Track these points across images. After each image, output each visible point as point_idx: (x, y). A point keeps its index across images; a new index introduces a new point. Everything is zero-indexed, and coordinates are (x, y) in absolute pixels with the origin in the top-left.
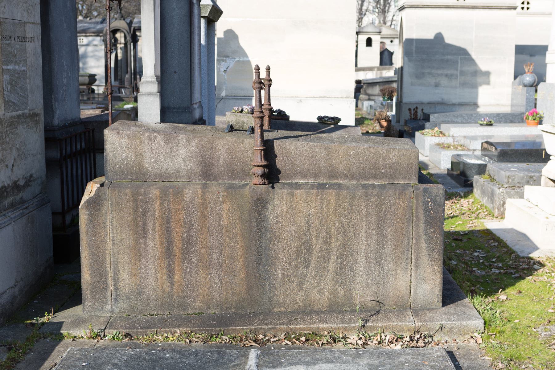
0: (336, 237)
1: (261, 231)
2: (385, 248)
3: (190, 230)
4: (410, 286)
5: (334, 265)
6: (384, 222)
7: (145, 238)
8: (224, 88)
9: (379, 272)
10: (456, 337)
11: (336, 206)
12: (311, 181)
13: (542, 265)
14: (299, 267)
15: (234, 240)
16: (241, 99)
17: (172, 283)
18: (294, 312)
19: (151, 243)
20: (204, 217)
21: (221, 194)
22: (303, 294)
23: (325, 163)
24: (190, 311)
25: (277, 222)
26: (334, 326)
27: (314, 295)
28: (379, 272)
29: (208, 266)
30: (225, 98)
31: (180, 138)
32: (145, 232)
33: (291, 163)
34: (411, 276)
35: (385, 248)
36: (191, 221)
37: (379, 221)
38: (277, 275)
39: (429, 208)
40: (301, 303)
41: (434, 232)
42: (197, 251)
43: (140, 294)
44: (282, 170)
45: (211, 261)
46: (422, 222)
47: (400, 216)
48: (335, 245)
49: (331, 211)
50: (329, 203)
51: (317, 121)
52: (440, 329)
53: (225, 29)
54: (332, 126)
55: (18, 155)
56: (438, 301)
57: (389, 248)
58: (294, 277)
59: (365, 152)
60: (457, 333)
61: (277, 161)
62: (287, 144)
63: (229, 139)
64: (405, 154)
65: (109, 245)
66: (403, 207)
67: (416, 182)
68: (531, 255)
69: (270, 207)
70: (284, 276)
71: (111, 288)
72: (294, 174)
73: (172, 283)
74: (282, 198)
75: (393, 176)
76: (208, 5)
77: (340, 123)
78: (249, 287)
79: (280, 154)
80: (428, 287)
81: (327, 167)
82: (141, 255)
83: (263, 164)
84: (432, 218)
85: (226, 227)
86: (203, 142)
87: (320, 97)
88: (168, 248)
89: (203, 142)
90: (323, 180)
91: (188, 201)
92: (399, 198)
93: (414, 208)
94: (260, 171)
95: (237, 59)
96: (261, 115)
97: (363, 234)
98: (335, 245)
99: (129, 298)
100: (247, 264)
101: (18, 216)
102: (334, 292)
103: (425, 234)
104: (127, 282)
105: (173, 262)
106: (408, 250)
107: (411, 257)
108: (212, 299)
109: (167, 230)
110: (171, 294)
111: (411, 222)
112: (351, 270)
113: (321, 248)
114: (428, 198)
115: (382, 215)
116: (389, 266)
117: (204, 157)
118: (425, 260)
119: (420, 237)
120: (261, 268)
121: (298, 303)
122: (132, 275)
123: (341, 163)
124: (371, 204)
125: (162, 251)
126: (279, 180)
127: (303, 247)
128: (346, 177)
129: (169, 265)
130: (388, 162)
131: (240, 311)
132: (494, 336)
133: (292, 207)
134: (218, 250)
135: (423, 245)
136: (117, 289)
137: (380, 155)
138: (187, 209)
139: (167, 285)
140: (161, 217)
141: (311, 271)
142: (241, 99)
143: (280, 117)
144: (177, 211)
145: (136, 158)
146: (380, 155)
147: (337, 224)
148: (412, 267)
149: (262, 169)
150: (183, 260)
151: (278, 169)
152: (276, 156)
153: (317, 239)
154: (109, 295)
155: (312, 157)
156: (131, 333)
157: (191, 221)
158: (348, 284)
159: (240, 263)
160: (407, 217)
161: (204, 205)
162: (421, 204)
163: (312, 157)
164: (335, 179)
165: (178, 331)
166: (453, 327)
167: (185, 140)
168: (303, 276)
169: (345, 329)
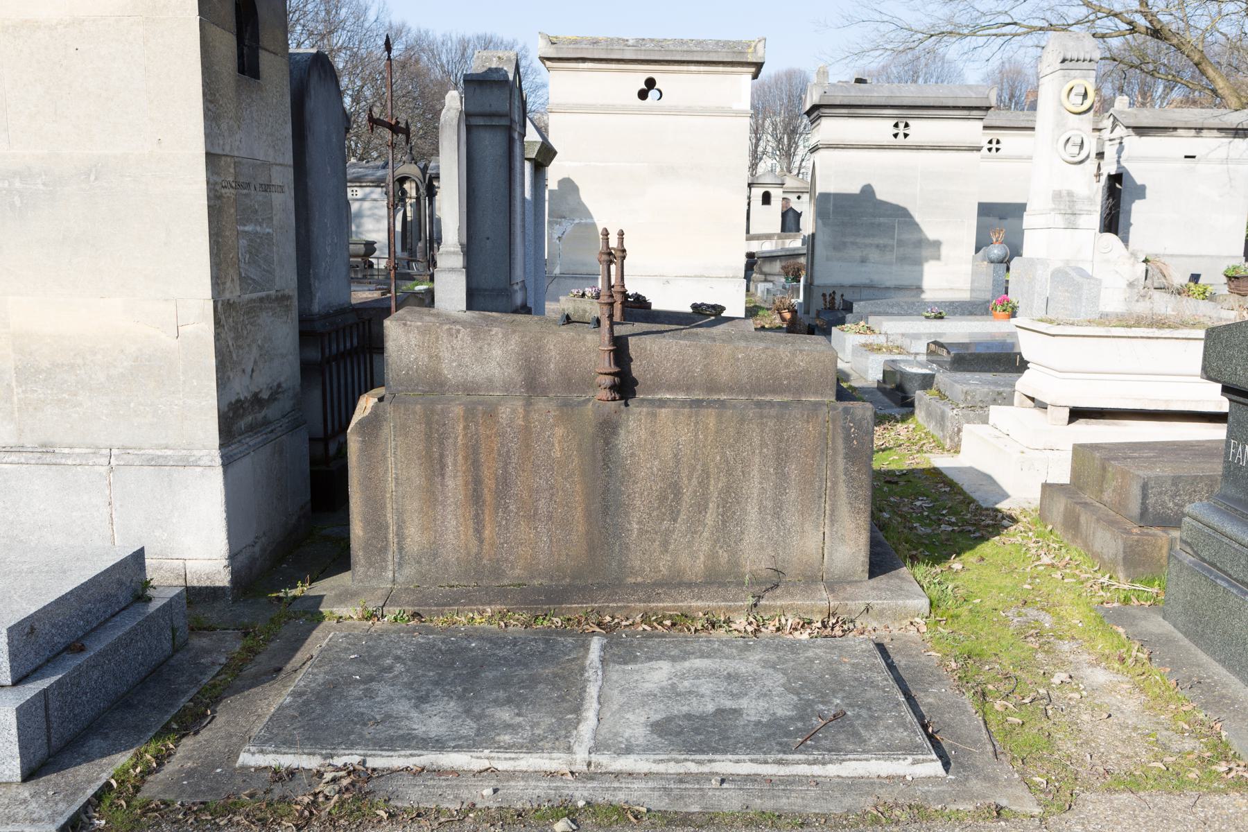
1: (608, 467)
4: (823, 549)
5: (714, 516)
7: (443, 475)
9: (779, 527)
10: (888, 622)
12: (681, 396)
13: (1014, 520)
14: (664, 520)
17: (481, 541)
19: (450, 483)
20: (528, 446)
22: (669, 559)
23: (702, 370)
24: (506, 582)
25: (633, 455)
27: (684, 561)
28: (779, 527)
29: (532, 517)
32: (443, 467)
34: (824, 533)
36: (508, 452)
37: (778, 454)
41: (858, 471)
43: (435, 555)
44: (640, 381)
45: (536, 509)
48: (715, 487)
49: (710, 439)
50: (707, 428)
53: (560, 178)
54: (713, 318)
56: (863, 571)
61: (632, 366)
63: (564, 334)
65: (391, 485)
67: (833, 399)
68: (998, 506)
69: (622, 432)
71: (393, 547)
72: (657, 387)
73: (481, 541)
75: (799, 391)
76: (535, 142)
79: (637, 357)
81: (705, 376)
82: (436, 500)
86: (527, 339)
87: (695, 276)
88: (475, 490)
89: (527, 339)
92: (808, 422)
93: (830, 436)
94: (608, 380)
95: (577, 221)
96: (610, 300)
97: (755, 473)
98: (715, 487)
102: (713, 556)
103: (845, 474)
106: (821, 497)
109: (474, 464)
110: (478, 557)
112: (737, 524)
113: (695, 492)
114: (850, 422)
115: (783, 445)
116: (792, 518)
117: (527, 360)
118: (844, 510)
120: (608, 520)
121: (660, 571)
122: (424, 529)
124: (767, 429)
126: (635, 395)
127: (669, 491)
128: (731, 390)
129: (477, 515)
130: (792, 369)
133: (653, 434)
134: (547, 494)
135: (842, 489)
136: (401, 549)
137: (782, 359)
140: (466, 446)
141: (680, 525)
144: (489, 437)
146: (782, 359)
147: (718, 458)
149: (612, 377)
152: (631, 360)
153: (690, 480)
154: (390, 558)
156: (421, 612)
157: (508, 452)
158: (733, 545)
159: (579, 514)
161: (527, 429)
164: (716, 394)
165: (489, 610)
166: (885, 609)
168: (669, 532)
169: (729, 609)
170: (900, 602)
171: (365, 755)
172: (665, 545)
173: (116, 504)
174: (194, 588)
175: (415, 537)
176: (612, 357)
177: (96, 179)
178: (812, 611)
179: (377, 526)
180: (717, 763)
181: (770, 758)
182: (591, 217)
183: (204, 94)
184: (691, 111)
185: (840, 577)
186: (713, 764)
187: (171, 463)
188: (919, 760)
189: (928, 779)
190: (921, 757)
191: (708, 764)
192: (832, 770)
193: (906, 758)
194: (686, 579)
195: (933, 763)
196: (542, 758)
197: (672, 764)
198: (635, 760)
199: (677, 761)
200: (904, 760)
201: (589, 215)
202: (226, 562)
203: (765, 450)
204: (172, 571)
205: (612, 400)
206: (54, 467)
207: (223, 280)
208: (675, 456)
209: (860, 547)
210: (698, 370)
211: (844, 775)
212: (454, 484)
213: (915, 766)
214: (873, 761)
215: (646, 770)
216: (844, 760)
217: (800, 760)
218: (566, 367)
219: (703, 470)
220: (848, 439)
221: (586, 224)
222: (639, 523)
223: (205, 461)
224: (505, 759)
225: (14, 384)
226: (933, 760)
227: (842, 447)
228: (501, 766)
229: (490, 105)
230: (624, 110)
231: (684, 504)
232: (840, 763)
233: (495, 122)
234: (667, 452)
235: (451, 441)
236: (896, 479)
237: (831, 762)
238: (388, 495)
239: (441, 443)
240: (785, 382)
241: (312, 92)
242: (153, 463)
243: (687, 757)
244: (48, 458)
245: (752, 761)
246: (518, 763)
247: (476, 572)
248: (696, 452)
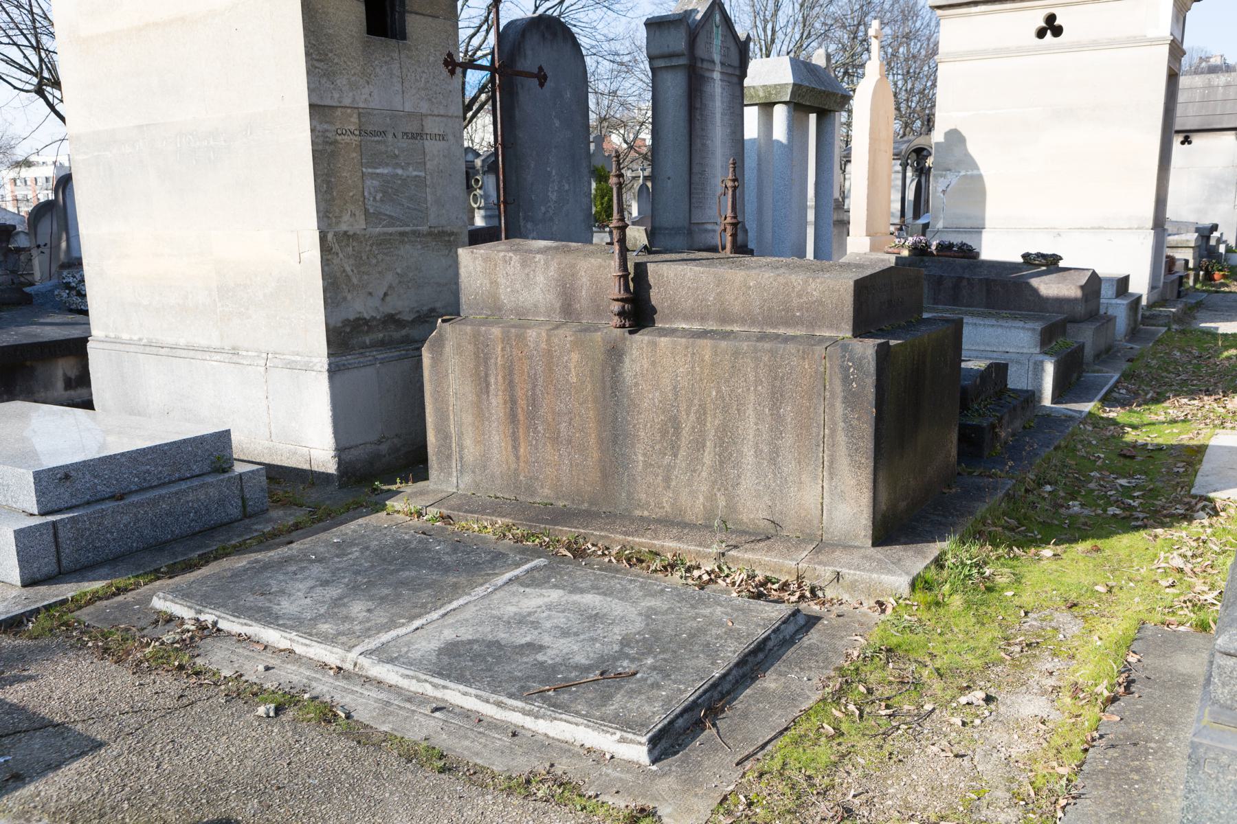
0: (712, 412)
1: (616, 395)
2: (783, 438)
3: (535, 386)
4: (822, 504)
5: (712, 455)
6: (781, 395)
7: (488, 392)
8: (942, 216)
9: (775, 475)
10: (863, 598)
11: (712, 365)
12: (696, 326)
13: (1215, 512)
14: (665, 454)
15: (584, 406)
16: (965, 232)
17: (518, 458)
18: (659, 521)
19: (494, 401)
20: (551, 370)
21: (569, 339)
22: (671, 495)
23: (715, 299)
24: (538, 500)
25: (636, 384)
26: (683, 546)
27: (684, 500)
28: (775, 475)
29: (555, 439)
30: (941, 231)
31: (537, 260)
32: (488, 385)
33: (670, 298)
34: (823, 487)
35: (783, 438)
36: (535, 374)
37: (773, 393)
38: (638, 462)
39: (849, 377)
40: (668, 508)
41: (858, 419)
42: (543, 416)
43: (485, 467)
44: (658, 308)
45: (559, 432)
46: (839, 400)
47: (805, 387)
48: (712, 425)
49: (706, 371)
50: (703, 360)
51: (1021, 260)
52: (836, 580)
53: (947, 130)
54: (1044, 268)
55: (400, 282)
56: (865, 536)
57: (789, 439)
58: (659, 467)
59: (771, 283)
60: (863, 592)
61: (651, 294)
62: (664, 269)
63: (593, 260)
64: (831, 286)
65: (452, 400)
66: (810, 372)
67: (849, 335)
68: (1212, 495)
69: (627, 360)
70: (647, 465)
71: (455, 456)
72: (676, 314)
73: (518, 458)
74: (642, 349)
75: (812, 324)
76: (787, 84)
77: (1062, 264)
78: (605, 476)
79: (655, 284)
80: (848, 509)
81: (718, 305)
82: (484, 415)
83: (620, 297)
84: (854, 394)
85: (575, 387)
86: (563, 265)
87: (1093, 228)
88: (512, 409)
89: (563, 265)
90: (711, 326)
91: (532, 346)
92: (804, 359)
93: (827, 377)
94: (616, 307)
95: (963, 173)
96: (620, 224)
97: (750, 412)
98: (712, 425)
99: (474, 472)
100: (601, 441)
101: (392, 357)
102: (711, 498)
103: (844, 421)
104: (472, 451)
105: (517, 428)
106: (819, 445)
107: (823, 457)
108: (561, 485)
109: (510, 385)
110: (516, 472)
111: (822, 399)
112: (734, 467)
113: (693, 428)
114: (848, 360)
115: (778, 383)
116: (789, 466)
117: (564, 286)
118: (843, 463)
119: (836, 424)
120: (617, 450)
121: (664, 507)
122: (477, 442)
123: (736, 299)
124: (762, 365)
125: (505, 412)
126: (654, 323)
127: (670, 425)
128: (743, 321)
129: (514, 433)
130: (805, 299)
131: (594, 509)
132: (916, 607)
133: (653, 364)
134: (566, 418)
135: (841, 438)
136: (461, 458)
137: (794, 287)
138: (531, 358)
139: (512, 458)
140: (504, 366)
141: (681, 462)
142: (965, 232)
143: (961, 254)
144: (520, 359)
145: (491, 287)
146: (794, 287)
147: (714, 393)
148: (825, 473)
149: (621, 304)
150: (528, 428)
151: (653, 306)
152: (650, 287)
153: (688, 415)
154: (454, 465)
155: (697, 289)
156: (452, 516)
157: (535, 374)
158: (730, 489)
159: (592, 440)
160: (815, 391)
161: (549, 352)
162: (837, 370)
163: (697, 289)
164: (729, 325)
165: (499, 522)
166: (857, 581)
167: (542, 262)
168: (669, 468)
169: (698, 553)
170: (875, 576)
171: (219, 617)
172: (667, 479)
173: (270, 398)
174: (315, 472)
175: (471, 451)
176: (622, 283)
177: (251, 133)
178: (781, 571)
179: (445, 437)
180: (449, 691)
181: (493, 697)
182: (978, 168)
183: (307, 54)
184: (1095, 45)
185: (840, 539)
186: (446, 691)
187: (299, 367)
188: (627, 738)
189: (629, 765)
190: (630, 736)
191: (442, 690)
192: (542, 726)
193: (615, 734)
194: (687, 520)
195: (639, 746)
196: (325, 650)
197: (414, 681)
198: (388, 670)
199: (419, 680)
200: (612, 734)
201: (974, 166)
202: (333, 453)
203: (760, 388)
204: (302, 456)
205: (620, 327)
206: (238, 366)
207: (337, 214)
208: (675, 388)
209: (862, 508)
210: (711, 299)
211: (551, 734)
212: (497, 402)
213: (620, 744)
214: (581, 728)
215: (393, 682)
216: (555, 719)
217: (517, 707)
218: (595, 293)
219: (700, 405)
220: (846, 380)
221: (972, 176)
222: (644, 455)
223: (318, 368)
224: (302, 644)
225: (217, 299)
226: (640, 743)
227: (840, 389)
228: (299, 650)
229: (668, 46)
230: (1020, 51)
231: (684, 439)
232: (551, 721)
233: (675, 62)
234: (666, 381)
235: (492, 361)
236: (1134, 452)
237: (543, 717)
238: (451, 408)
239: (486, 363)
240: (798, 314)
241: (529, 53)
242: (289, 366)
243: (428, 677)
244: (235, 358)
245: (477, 696)
246: (309, 649)
247: (516, 487)
248: (693, 384)
